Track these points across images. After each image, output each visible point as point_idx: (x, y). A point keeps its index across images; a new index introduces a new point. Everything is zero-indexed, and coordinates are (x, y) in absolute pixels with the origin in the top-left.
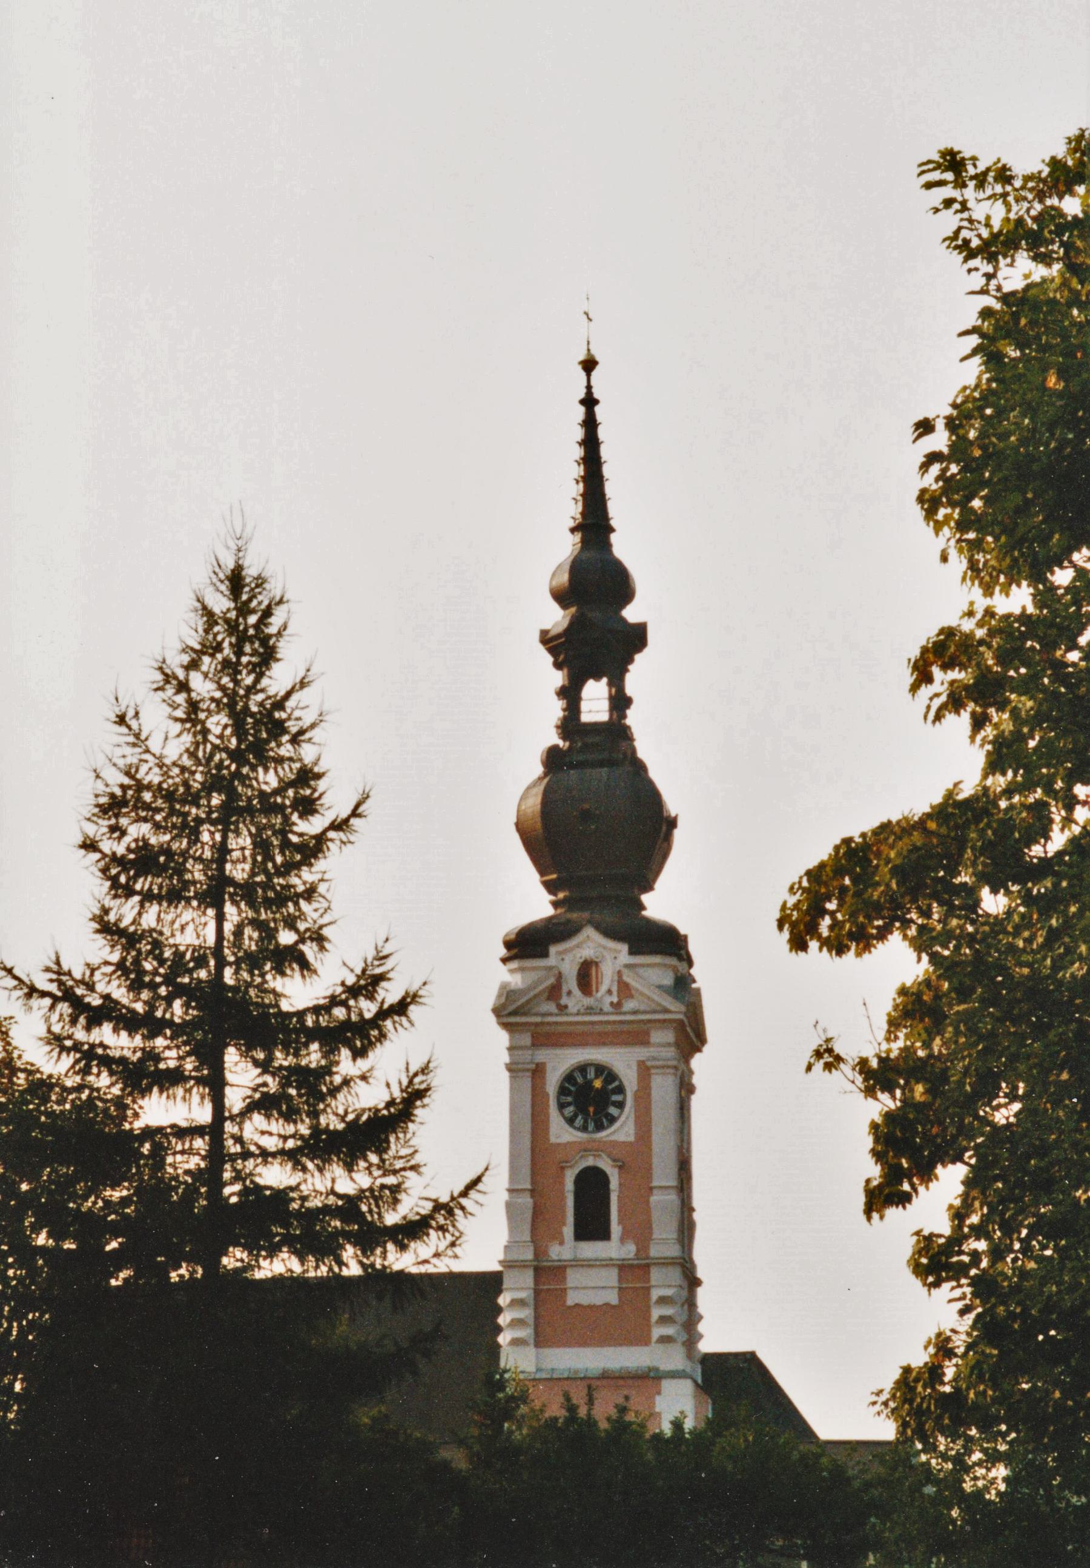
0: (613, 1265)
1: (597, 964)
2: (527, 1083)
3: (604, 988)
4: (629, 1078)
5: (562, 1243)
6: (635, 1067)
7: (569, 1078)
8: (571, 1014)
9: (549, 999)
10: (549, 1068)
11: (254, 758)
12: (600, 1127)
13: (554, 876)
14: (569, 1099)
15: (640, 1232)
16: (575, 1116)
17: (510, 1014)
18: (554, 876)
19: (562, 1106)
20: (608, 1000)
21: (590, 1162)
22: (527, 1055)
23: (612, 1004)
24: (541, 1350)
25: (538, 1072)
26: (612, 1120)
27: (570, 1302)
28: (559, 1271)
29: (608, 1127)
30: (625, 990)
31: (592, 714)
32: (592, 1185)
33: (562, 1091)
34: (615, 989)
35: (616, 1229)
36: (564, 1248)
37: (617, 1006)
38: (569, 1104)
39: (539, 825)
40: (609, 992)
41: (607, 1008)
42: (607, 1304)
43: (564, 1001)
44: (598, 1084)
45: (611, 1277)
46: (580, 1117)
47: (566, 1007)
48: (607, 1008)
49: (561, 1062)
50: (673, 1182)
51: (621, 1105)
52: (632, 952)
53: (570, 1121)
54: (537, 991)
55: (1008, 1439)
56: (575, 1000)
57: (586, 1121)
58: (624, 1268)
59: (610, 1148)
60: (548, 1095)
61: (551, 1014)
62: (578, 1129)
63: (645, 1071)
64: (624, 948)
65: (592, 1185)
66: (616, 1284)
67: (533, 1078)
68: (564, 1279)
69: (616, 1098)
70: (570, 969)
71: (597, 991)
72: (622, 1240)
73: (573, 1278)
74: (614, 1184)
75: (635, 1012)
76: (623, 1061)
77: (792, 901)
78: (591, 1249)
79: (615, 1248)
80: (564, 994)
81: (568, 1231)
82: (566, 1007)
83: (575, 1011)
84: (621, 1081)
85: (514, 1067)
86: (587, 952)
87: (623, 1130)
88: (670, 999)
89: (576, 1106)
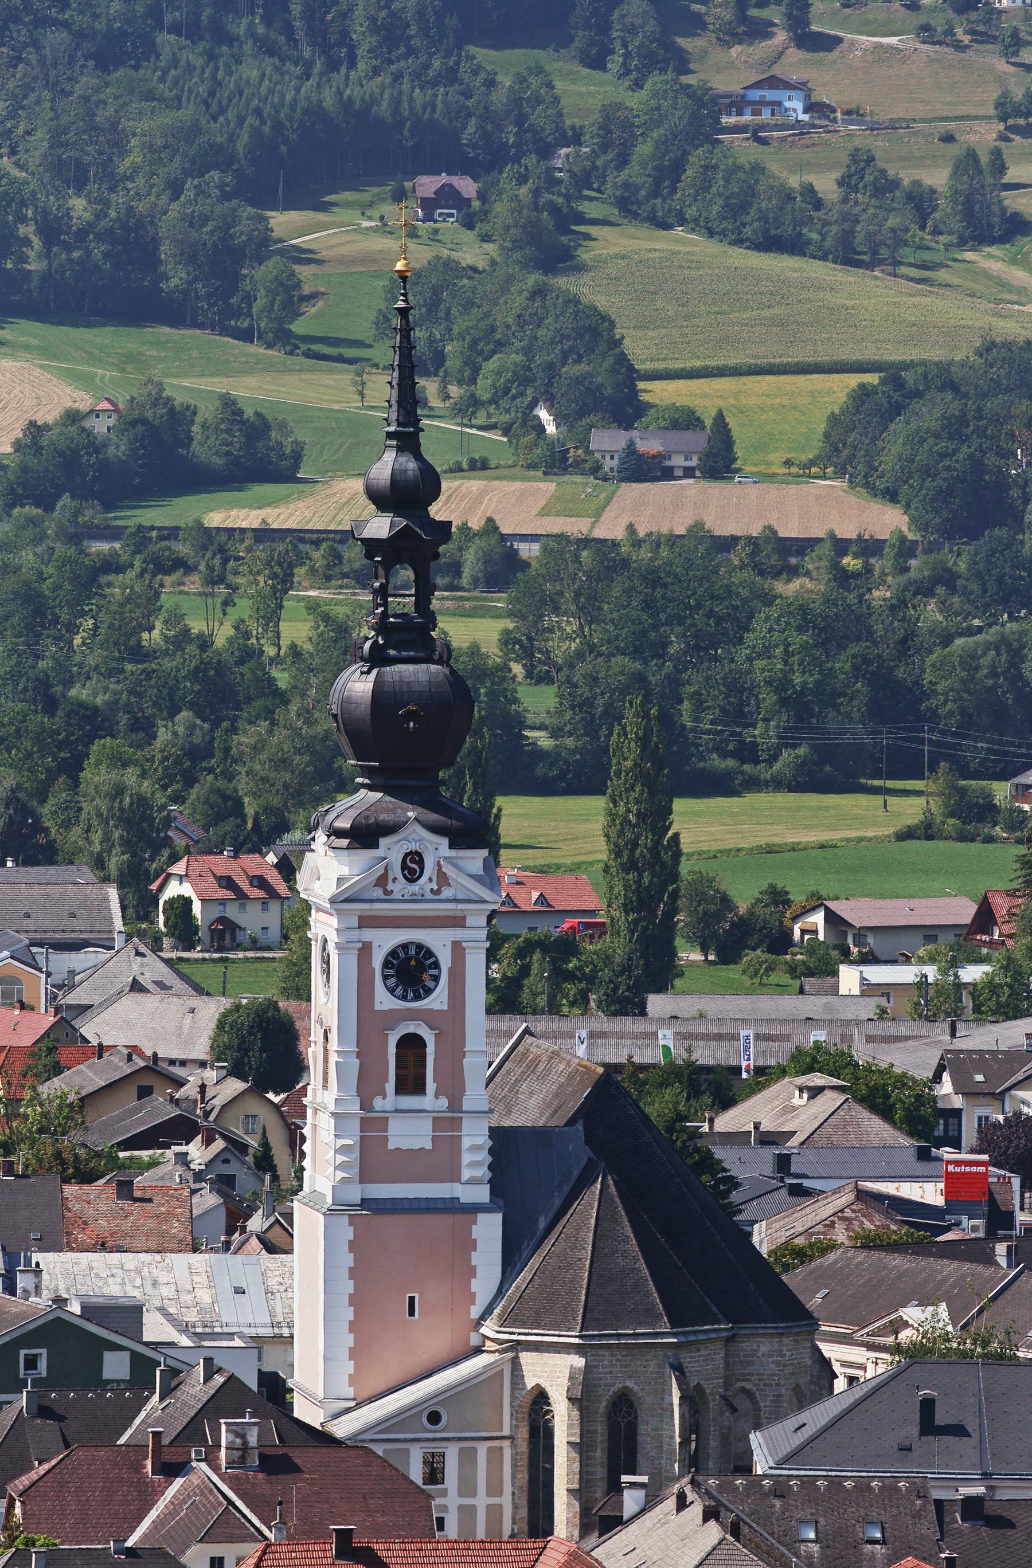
2: (353, 959)
7: (393, 953)
10: (375, 946)
11: (277, 1093)
14: (392, 972)
19: (385, 978)
21: (412, 1029)
22: (355, 935)
25: (365, 950)
26: (429, 991)
27: (391, 1146)
28: (383, 1123)
30: (443, 879)
32: (412, 1045)
33: (386, 964)
35: (431, 1086)
36: (388, 1101)
39: (369, 722)
40: (430, 880)
41: (429, 895)
42: (423, 1149)
43: (389, 887)
45: (426, 1126)
49: (385, 941)
51: (436, 979)
53: (392, 991)
56: (399, 887)
57: (405, 991)
59: (429, 1018)
63: (458, 949)
64: (445, 842)
65: (412, 1045)
70: (396, 858)
72: (436, 1096)
74: (430, 1049)
76: (439, 942)
78: (409, 1102)
79: (431, 1100)
81: (390, 1086)
86: (413, 847)
87: (438, 1000)
88: (488, 891)
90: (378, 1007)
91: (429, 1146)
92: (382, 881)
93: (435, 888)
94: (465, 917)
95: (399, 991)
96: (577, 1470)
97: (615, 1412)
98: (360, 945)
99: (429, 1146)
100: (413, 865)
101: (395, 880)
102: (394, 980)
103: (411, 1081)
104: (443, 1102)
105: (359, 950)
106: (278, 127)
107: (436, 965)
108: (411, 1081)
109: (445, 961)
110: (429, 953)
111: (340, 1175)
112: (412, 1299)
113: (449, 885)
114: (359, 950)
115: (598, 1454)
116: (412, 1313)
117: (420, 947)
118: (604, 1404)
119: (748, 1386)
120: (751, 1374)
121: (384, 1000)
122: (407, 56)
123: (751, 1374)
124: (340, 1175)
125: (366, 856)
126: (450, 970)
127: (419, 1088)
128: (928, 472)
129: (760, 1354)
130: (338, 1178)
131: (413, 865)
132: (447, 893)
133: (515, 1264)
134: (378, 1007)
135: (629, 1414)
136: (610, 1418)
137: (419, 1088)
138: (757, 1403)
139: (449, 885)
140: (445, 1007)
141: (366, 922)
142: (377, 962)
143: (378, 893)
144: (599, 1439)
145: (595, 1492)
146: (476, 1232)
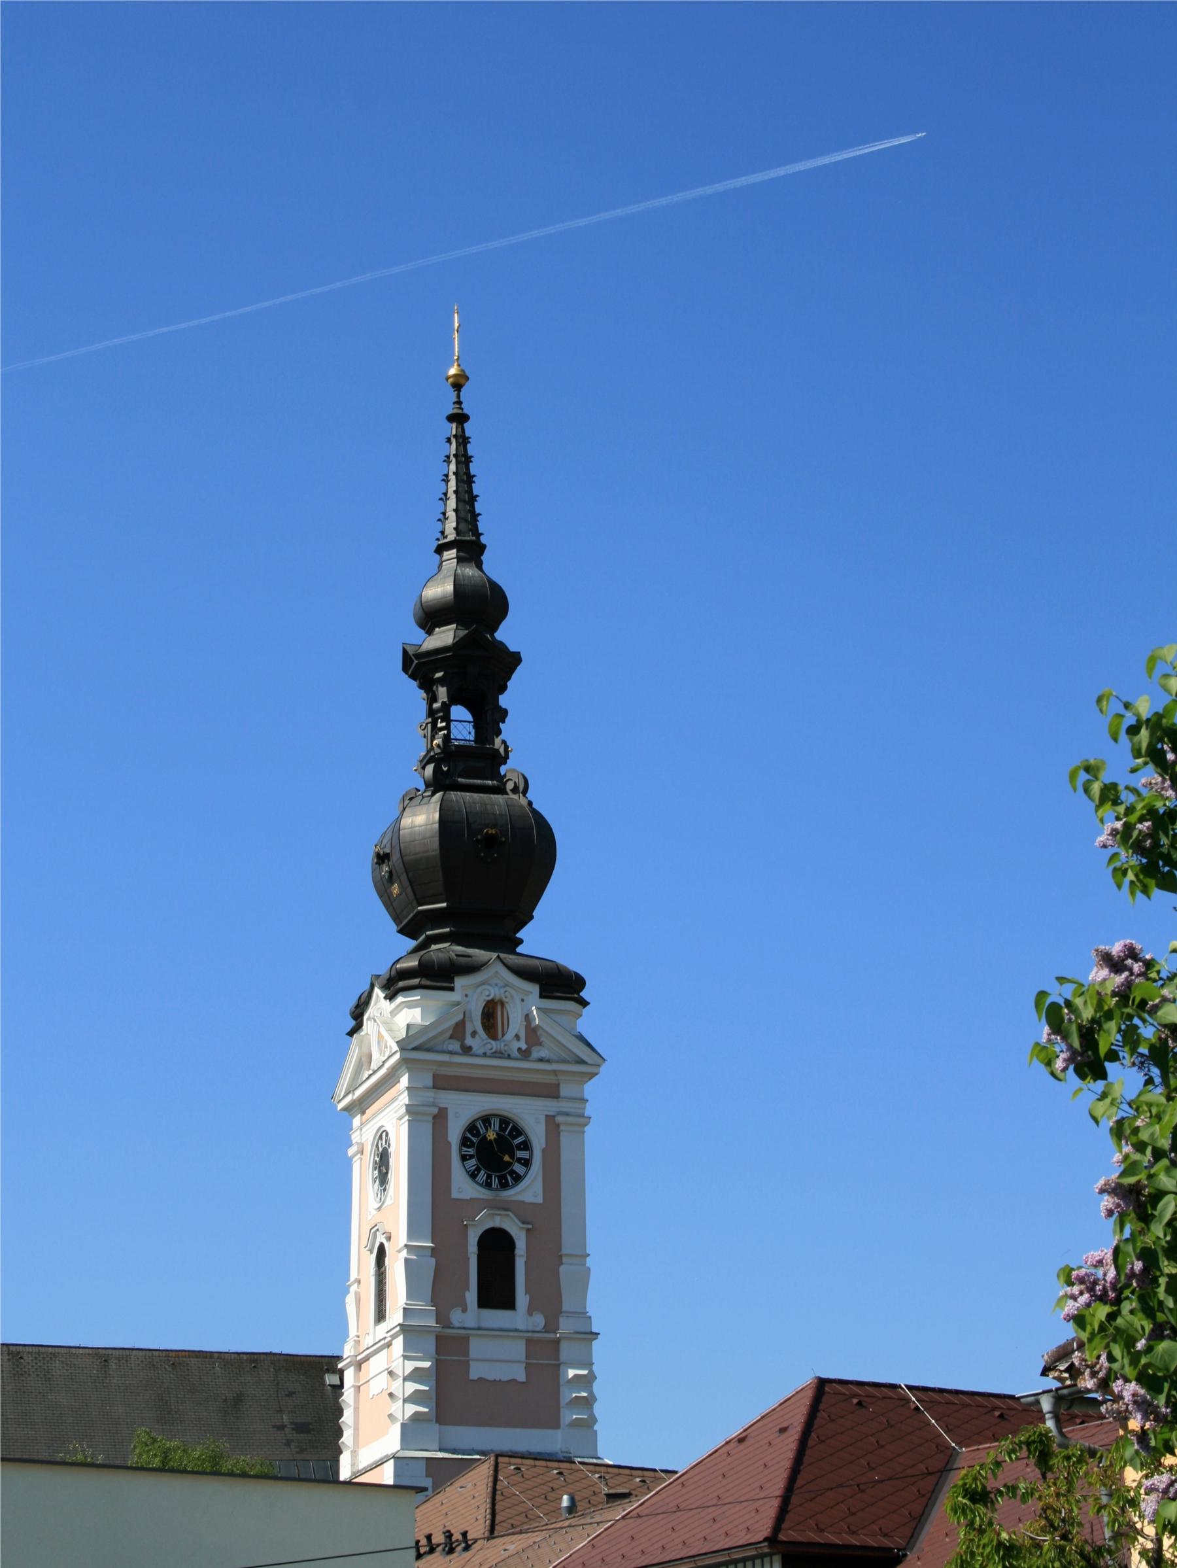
0: (520, 1337)
1: (502, 1004)
2: (427, 1128)
3: (510, 1035)
4: (537, 1136)
5: (464, 1310)
6: (543, 1120)
7: (472, 1128)
8: (476, 1056)
12: (504, 1186)
13: (444, 905)
14: (472, 1151)
15: (550, 1303)
16: (478, 1170)
18: (444, 905)
19: (464, 1158)
20: (516, 1045)
21: (497, 1222)
23: (519, 1049)
24: (443, 1427)
25: (440, 1118)
26: (518, 1178)
29: (514, 1186)
33: (465, 1142)
34: (523, 1036)
36: (469, 1314)
37: (525, 1054)
38: (471, 1157)
40: (517, 1037)
41: (515, 1053)
43: (469, 1041)
44: (491, 1136)
45: (517, 1349)
46: (482, 1172)
48: (515, 1053)
49: (465, 1109)
51: (527, 1163)
53: (473, 1176)
54: (440, 1029)
55: (585, 1372)
56: (479, 1041)
57: (489, 1177)
59: (522, 1211)
60: (449, 1143)
62: (481, 1185)
64: (535, 989)
65: (496, 1249)
66: (523, 1358)
68: (466, 1352)
71: (503, 1035)
72: (530, 1312)
73: (477, 1347)
75: (541, 1060)
78: (496, 1317)
81: (472, 1296)
82: (470, 1048)
83: (481, 1051)
84: (526, 1136)
85: (581, 1120)
86: (494, 993)
87: (530, 1190)
89: (479, 1159)
90: (455, 1194)
91: (522, 1378)
92: (458, 1030)
93: (524, 1047)
94: (466, 1339)
98: (435, 1110)
99: (522, 1378)
100: (491, 1015)
101: (474, 1034)
102: (473, 1162)
103: (496, 1291)
104: (539, 1320)
105: (435, 1117)
106: (1169, 1522)
107: (526, 1146)
108: (496, 1291)
109: (538, 1141)
110: (517, 1131)
111: (411, 1409)
113: (540, 1044)
114: (435, 1117)
117: (504, 1121)
121: (463, 1186)
124: (411, 1409)
125: (441, 998)
126: (544, 1150)
127: (508, 1303)
130: (408, 1414)
131: (491, 1015)
132: (537, 1053)
134: (455, 1194)
137: (508, 1303)
139: (540, 1044)
140: (540, 1200)
141: (441, 1083)
143: (455, 1046)
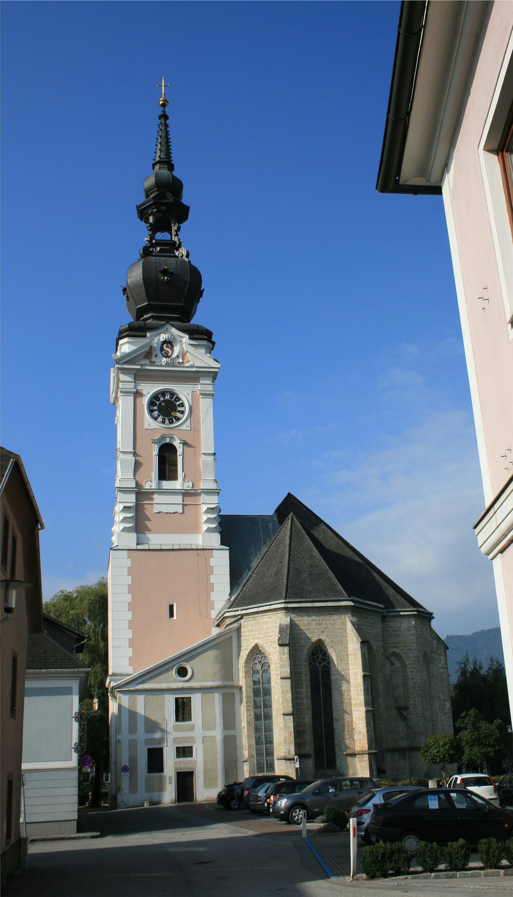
9: (145, 358)
17: (126, 363)
31: (493, 513)
33: (151, 403)
46: (160, 417)
47: (154, 362)
49: (149, 389)
50: (150, 548)
51: (182, 412)
52: (190, 339)
57: (164, 419)
58: (185, 494)
61: (147, 365)
64: (187, 336)
67: (134, 397)
69: (179, 409)
74: (180, 451)
77: (151, 233)
78: (166, 485)
80: (153, 356)
82: (154, 362)
87: (184, 424)
95: (160, 419)
96: (290, 699)
97: (313, 659)
101: (156, 356)
112: (171, 607)
115: (304, 690)
116: (171, 615)
118: (306, 652)
119: (397, 651)
120: (398, 643)
122: (99, 606)
123: (398, 643)
128: (348, 726)
129: (402, 629)
133: (239, 585)
135: (324, 660)
136: (310, 664)
138: (404, 662)
142: (145, 401)
144: (304, 678)
145: (304, 718)
146: (212, 562)
